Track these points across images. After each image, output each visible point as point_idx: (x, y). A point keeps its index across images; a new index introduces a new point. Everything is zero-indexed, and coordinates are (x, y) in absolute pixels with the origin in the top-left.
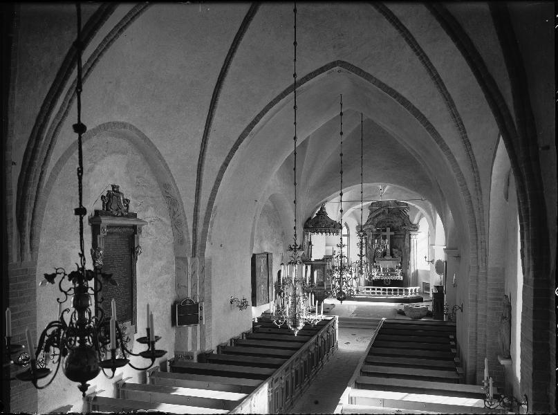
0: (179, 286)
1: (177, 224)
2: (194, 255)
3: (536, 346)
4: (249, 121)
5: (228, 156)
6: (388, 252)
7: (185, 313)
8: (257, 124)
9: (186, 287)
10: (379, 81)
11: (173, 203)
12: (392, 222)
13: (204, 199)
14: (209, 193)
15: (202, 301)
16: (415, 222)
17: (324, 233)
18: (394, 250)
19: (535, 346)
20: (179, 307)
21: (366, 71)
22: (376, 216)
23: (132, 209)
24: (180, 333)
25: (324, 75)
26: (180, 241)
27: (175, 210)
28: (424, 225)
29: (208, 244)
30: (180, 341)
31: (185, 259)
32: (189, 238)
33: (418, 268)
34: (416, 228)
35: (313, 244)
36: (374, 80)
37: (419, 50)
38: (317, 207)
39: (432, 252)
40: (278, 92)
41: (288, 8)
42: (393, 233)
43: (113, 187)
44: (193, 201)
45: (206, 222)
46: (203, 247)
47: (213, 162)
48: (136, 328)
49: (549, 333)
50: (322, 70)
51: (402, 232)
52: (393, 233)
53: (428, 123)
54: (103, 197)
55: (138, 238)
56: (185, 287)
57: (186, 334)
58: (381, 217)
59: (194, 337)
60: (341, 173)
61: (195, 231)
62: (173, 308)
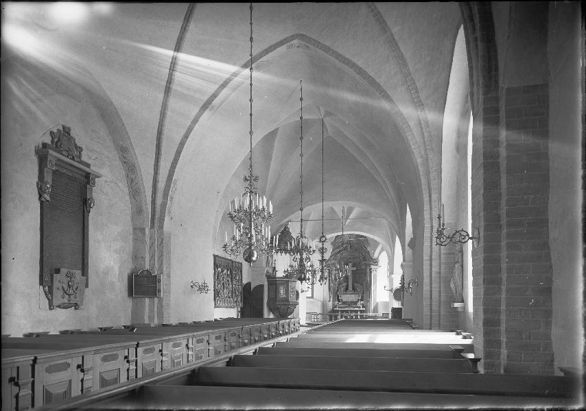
0: (136, 256)
1: (135, 192)
3: (487, 282)
7: (143, 284)
9: (143, 258)
10: (336, 52)
11: (131, 169)
14: (169, 166)
15: (161, 273)
18: (356, 284)
22: (339, 252)
23: (84, 158)
24: (137, 304)
25: (283, 49)
26: (138, 211)
28: (383, 259)
29: (167, 219)
30: (136, 312)
34: (376, 262)
35: (277, 269)
36: (331, 52)
39: (391, 281)
41: (248, 5)
42: (355, 269)
43: (64, 127)
45: (166, 195)
46: (162, 220)
48: (87, 280)
49: (498, 150)
50: (281, 43)
52: (355, 269)
54: (52, 133)
56: (142, 257)
58: (345, 254)
59: (151, 311)
61: (154, 202)
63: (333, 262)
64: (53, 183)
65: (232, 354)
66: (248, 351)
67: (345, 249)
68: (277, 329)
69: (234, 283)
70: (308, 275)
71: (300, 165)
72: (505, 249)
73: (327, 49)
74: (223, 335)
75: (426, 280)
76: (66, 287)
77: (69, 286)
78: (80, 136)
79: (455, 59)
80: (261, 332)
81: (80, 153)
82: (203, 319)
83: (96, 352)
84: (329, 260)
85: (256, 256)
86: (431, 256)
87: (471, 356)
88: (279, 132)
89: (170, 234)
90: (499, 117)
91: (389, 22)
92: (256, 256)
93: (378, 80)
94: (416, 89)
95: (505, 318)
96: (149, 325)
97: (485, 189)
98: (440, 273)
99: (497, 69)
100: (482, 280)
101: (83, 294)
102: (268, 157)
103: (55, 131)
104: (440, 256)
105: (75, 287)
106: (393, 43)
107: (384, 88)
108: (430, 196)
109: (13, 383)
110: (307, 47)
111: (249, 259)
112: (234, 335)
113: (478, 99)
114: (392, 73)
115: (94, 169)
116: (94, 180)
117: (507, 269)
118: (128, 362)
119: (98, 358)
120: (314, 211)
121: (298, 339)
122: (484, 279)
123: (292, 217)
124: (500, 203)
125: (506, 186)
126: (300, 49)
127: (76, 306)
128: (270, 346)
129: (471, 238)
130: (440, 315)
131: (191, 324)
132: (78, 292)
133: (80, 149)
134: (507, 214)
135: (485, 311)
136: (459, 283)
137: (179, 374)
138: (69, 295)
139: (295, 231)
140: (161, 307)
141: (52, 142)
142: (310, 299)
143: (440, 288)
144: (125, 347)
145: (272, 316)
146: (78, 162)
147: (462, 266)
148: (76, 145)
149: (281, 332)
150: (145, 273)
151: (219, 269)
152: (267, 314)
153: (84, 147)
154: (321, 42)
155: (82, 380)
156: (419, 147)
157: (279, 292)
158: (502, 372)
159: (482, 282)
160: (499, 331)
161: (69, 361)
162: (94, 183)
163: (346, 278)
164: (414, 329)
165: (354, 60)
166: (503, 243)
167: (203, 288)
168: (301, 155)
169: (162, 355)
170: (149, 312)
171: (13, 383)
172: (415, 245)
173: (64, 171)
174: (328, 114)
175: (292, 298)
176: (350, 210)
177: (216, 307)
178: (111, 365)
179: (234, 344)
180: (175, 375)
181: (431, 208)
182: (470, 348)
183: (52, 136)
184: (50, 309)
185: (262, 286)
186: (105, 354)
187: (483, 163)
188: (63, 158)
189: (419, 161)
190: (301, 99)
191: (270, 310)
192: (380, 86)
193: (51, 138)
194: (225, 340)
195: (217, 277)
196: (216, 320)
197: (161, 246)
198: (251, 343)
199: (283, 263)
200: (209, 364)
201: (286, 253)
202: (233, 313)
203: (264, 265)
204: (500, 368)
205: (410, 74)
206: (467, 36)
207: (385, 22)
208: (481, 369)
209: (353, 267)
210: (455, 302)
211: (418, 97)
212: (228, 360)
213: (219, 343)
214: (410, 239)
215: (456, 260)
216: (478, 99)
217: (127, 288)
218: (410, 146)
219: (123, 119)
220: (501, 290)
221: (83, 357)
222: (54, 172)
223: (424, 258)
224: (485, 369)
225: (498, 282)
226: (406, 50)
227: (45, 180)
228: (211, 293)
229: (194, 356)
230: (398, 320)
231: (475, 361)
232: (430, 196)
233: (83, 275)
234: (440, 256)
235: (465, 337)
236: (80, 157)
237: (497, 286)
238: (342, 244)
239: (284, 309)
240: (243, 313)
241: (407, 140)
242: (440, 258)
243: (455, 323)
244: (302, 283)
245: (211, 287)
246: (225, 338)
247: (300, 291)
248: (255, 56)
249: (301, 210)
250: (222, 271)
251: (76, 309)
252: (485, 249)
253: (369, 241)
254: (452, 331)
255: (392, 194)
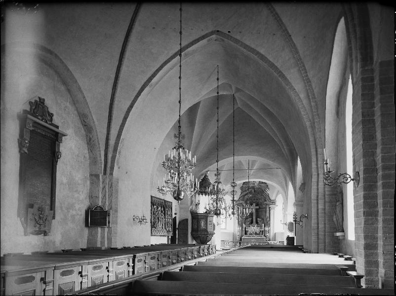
0: (91, 197)
2: (105, 173)
4: (149, 75)
5: (133, 101)
6: (254, 220)
7: (97, 217)
8: (156, 77)
12: (257, 199)
13: (110, 156)
16: (272, 198)
17: (207, 196)
18: (258, 219)
19: (363, 122)
20: (92, 211)
21: (235, 37)
22: (246, 195)
25: (205, 41)
26: (94, 161)
27: (91, 137)
28: (279, 200)
29: (116, 168)
30: (91, 239)
31: (97, 176)
32: (101, 160)
33: (276, 231)
34: (273, 202)
37: (272, 10)
38: (202, 175)
40: (171, 54)
41: (178, 6)
42: (258, 207)
44: (105, 131)
45: (115, 150)
46: (112, 168)
47: (121, 105)
49: (374, 110)
50: (203, 38)
51: (264, 206)
52: (258, 207)
53: (280, 72)
55: (59, 145)
57: (97, 233)
59: (103, 237)
60: (218, 108)
62: (87, 212)
63: (241, 202)
64: (30, 140)
65: (163, 270)
66: (176, 268)
67: (250, 193)
68: (199, 252)
69: (166, 217)
70: (223, 211)
71: (216, 128)
72: (381, 188)
73: (237, 41)
74: (156, 257)
75: (314, 215)
76: (37, 218)
77: (40, 218)
78: (51, 105)
79: (335, 46)
80: (178, 256)
81: (51, 118)
82: (142, 244)
83: (89, 264)
84: (238, 200)
85: (183, 195)
86: (317, 197)
87: (353, 273)
88: (201, 105)
89: (118, 179)
90: (374, 84)
91: (285, 20)
92: (183, 195)
93: (276, 64)
94: (305, 69)
95: (382, 243)
96: (101, 248)
97: (363, 141)
98: (325, 209)
99: (371, 47)
100: (362, 212)
101: (50, 224)
102: (192, 123)
103: (33, 101)
104: (324, 196)
105: (45, 218)
106: (288, 36)
107: (281, 69)
108: (316, 151)
109: (42, 282)
110: (223, 40)
111: (177, 198)
112: (165, 256)
113: (357, 72)
114: (287, 58)
115: (61, 130)
116: (61, 138)
117: (383, 204)
118: (81, 276)
119: (90, 267)
120: (226, 163)
121: (214, 260)
122: (364, 212)
123: (210, 168)
124: (376, 152)
125: (380, 138)
126: (217, 42)
127: (45, 233)
128: (193, 264)
129: (353, 180)
130: (325, 243)
131: (142, 247)
132: (47, 222)
133: (51, 115)
134: (382, 159)
135: (366, 237)
136: (340, 216)
137: (120, 285)
138: (40, 225)
139: (212, 179)
140: (110, 232)
141: (30, 109)
142: (225, 227)
143: (325, 221)
144: (79, 265)
145: (194, 242)
146: (50, 124)
147: (342, 204)
148: (48, 112)
149: (190, 257)
150: (98, 209)
151: (155, 207)
152: (190, 241)
153: (54, 113)
154: (233, 36)
155: (81, 283)
156: (307, 114)
157: (200, 225)
158: (380, 286)
159: (362, 215)
160: (377, 254)
161: (34, 275)
162: (61, 140)
163: (251, 214)
164: (305, 252)
165: (258, 49)
166: (380, 183)
167: (142, 221)
168: (218, 121)
169: (108, 271)
170: (101, 236)
171: (42, 282)
172: (304, 187)
173: (39, 131)
174: (238, 90)
175: (210, 229)
176: (254, 162)
177: (152, 235)
178: (68, 279)
179: (165, 264)
180: (114, 287)
181: (317, 160)
182: (353, 268)
183: (31, 106)
184: (25, 235)
185: (187, 220)
186: (63, 270)
187: (362, 120)
188: (38, 121)
189: (308, 124)
190: (218, 79)
191: (194, 238)
192: (277, 68)
193: (29, 106)
194: (158, 260)
195: (153, 213)
196: (152, 245)
197: (112, 189)
198: (178, 262)
199: (204, 203)
200: (143, 278)
201: (205, 195)
202: (164, 240)
203: (189, 203)
204: (378, 284)
205: (301, 59)
206: (347, 24)
207: (281, 20)
208: (363, 283)
209: (255, 206)
210: (336, 232)
211: (307, 76)
212: (159, 275)
213: (154, 263)
214: (300, 184)
215: (337, 198)
216: (357, 72)
217: (238, 266)
218: (300, 113)
219: (84, 93)
220: (377, 220)
221: (45, 272)
222: (32, 132)
223: (312, 198)
224: (366, 284)
225: (375, 214)
226: (298, 40)
227: (25, 137)
228: (149, 224)
229: (149, 268)
230: (291, 246)
231: (359, 278)
232: (316, 151)
233: (51, 210)
234: (324, 196)
235: (346, 259)
236: (51, 120)
237: (375, 218)
238: (248, 189)
239: (203, 237)
240: (173, 240)
241: (299, 108)
242: (325, 198)
243: (337, 247)
244: (217, 217)
245: (149, 221)
246: (158, 258)
247: (216, 224)
248: (184, 47)
249: (217, 162)
250: (158, 208)
251: (45, 235)
252: (364, 188)
253: (269, 187)
254: (335, 254)
255: (285, 151)
